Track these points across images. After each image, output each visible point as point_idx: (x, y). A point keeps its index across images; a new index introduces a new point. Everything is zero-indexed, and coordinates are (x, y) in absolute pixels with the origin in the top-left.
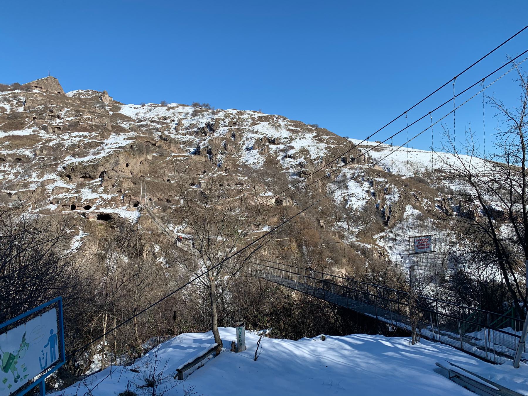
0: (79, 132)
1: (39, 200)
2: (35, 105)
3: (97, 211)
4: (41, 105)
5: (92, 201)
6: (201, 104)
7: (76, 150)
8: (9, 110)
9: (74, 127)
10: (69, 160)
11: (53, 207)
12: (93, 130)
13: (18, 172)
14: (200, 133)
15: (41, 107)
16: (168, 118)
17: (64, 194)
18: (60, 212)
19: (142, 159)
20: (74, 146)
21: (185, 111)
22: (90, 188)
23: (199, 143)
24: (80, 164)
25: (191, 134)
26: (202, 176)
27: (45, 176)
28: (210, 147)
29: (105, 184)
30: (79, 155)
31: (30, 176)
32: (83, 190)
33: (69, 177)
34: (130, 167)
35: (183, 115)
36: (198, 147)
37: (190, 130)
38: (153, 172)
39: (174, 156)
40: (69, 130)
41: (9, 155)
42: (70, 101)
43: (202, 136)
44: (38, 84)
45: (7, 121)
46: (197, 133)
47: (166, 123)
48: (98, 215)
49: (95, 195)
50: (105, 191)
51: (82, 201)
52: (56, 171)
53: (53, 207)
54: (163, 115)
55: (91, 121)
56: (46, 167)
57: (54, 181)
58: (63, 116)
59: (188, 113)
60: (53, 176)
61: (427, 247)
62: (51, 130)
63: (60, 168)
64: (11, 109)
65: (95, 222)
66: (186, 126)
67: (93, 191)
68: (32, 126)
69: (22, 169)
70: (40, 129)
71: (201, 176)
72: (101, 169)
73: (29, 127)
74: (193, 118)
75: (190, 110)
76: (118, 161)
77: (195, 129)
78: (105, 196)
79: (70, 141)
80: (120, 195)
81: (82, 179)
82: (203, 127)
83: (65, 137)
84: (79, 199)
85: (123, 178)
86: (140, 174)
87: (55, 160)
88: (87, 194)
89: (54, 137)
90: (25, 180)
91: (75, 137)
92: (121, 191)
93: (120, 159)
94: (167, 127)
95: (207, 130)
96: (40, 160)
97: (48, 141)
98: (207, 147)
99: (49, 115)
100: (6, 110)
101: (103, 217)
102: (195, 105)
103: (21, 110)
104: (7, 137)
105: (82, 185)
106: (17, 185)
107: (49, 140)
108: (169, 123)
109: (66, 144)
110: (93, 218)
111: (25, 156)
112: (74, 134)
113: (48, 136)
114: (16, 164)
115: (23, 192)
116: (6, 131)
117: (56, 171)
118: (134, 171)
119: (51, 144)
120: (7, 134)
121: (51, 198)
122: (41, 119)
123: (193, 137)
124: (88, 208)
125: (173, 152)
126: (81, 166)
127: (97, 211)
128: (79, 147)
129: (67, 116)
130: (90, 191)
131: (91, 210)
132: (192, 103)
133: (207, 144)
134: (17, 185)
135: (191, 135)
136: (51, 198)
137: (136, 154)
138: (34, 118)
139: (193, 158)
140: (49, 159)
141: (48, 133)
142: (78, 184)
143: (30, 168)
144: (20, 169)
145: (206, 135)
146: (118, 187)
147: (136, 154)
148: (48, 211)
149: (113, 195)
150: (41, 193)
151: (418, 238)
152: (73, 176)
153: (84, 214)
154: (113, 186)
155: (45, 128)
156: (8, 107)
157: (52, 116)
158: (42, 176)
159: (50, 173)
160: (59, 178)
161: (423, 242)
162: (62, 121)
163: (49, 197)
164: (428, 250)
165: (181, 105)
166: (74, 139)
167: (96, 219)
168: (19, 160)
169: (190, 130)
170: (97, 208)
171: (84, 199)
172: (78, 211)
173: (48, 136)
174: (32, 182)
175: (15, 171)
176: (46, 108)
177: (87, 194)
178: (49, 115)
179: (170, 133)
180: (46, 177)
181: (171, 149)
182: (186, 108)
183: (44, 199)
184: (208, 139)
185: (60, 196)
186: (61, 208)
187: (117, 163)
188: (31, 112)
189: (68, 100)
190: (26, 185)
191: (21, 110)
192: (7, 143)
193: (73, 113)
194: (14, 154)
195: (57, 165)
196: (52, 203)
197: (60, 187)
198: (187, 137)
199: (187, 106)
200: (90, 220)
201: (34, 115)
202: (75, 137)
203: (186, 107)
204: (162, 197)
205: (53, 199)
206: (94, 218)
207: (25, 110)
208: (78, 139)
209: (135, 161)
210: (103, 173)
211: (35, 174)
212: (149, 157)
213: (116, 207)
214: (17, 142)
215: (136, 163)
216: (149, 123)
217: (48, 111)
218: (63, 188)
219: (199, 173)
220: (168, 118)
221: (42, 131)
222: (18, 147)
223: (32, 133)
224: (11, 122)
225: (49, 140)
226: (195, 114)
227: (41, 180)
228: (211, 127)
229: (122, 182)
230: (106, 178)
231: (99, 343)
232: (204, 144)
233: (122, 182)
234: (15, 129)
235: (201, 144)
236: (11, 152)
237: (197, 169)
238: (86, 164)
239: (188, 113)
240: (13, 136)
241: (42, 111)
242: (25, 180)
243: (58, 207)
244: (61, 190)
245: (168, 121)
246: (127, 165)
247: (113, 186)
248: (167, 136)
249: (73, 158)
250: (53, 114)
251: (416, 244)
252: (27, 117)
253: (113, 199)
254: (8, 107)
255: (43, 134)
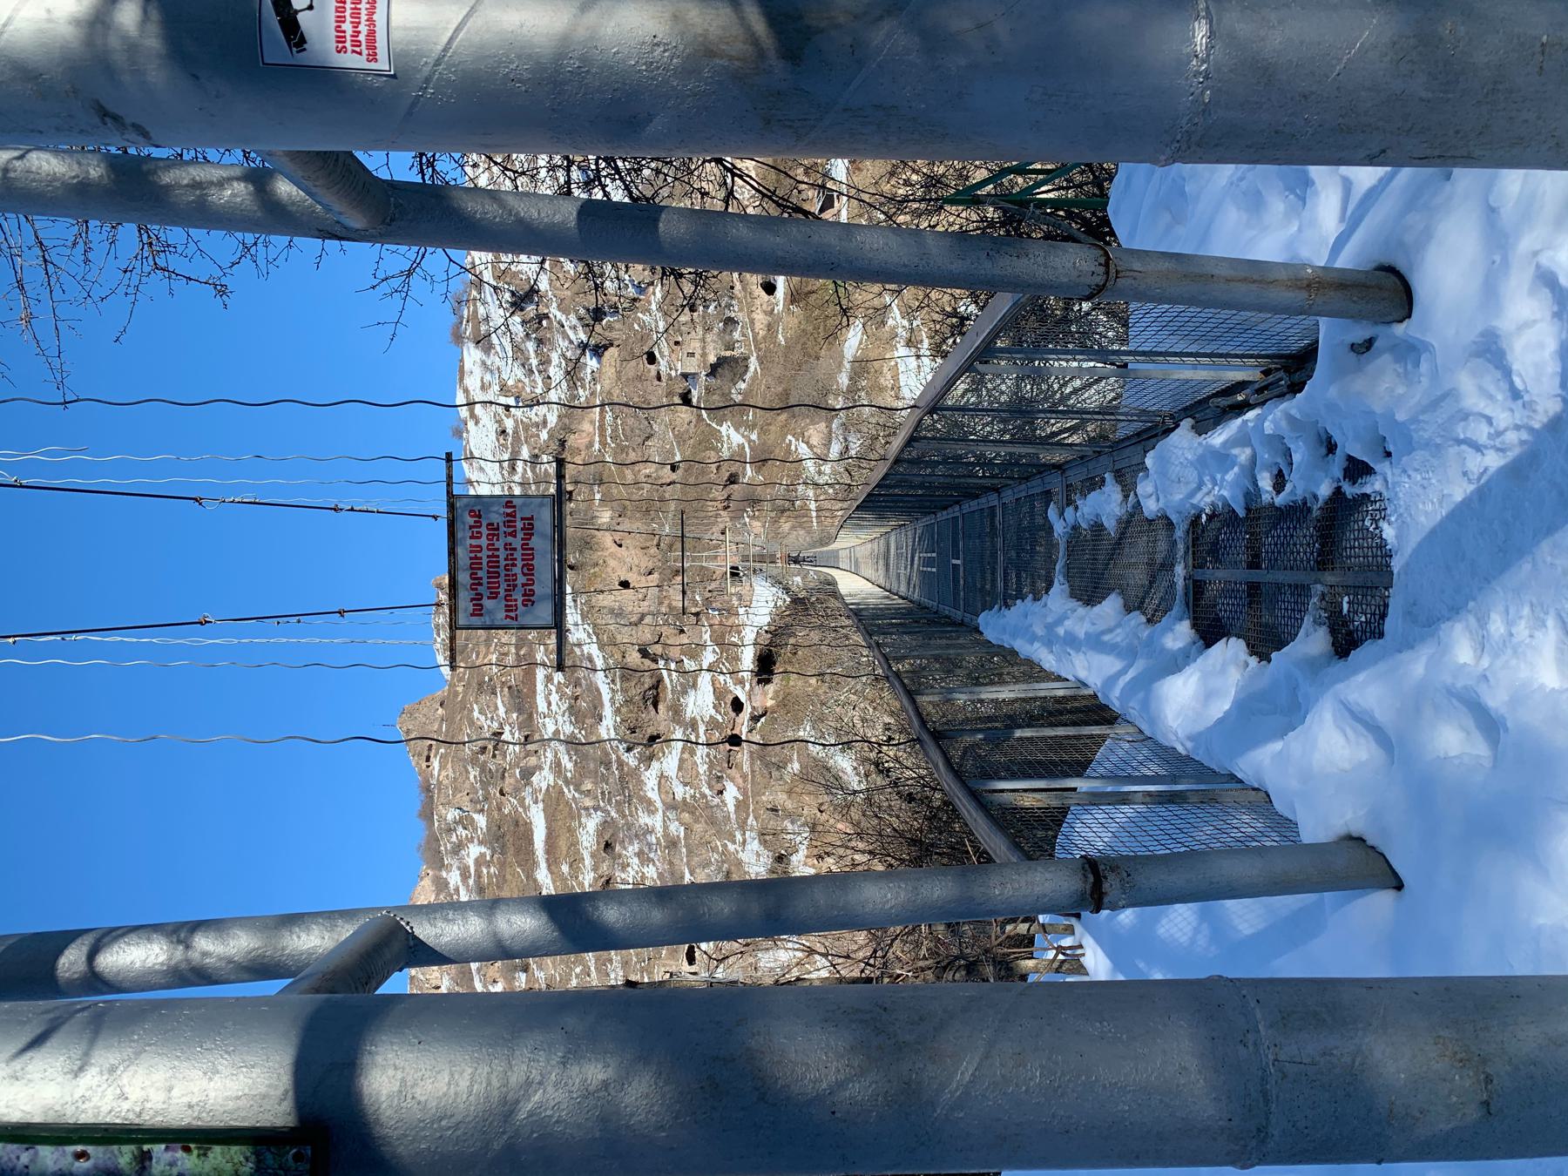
0: (535, 692)
1: (712, 821)
2: (467, 785)
3: (747, 687)
4: (467, 772)
5: (719, 693)
6: (454, 319)
7: (584, 710)
8: (483, 849)
9: (522, 700)
10: (607, 728)
11: (731, 793)
12: (531, 653)
13: (640, 854)
14: (541, 334)
15: (473, 773)
16: (500, 422)
17: (699, 761)
18: (744, 777)
19: (607, 539)
20: (572, 710)
21: (478, 371)
22: (684, 692)
23: (571, 342)
24: (617, 711)
25: (545, 362)
26: (663, 364)
27: (649, 794)
28: (582, 311)
29: (675, 653)
30: (597, 704)
31: (651, 831)
32: (689, 711)
33: (653, 739)
34: (632, 578)
35: (488, 377)
36: (584, 347)
37: (534, 362)
38: (648, 508)
39: (603, 443)
40: (531, 716)
41: (595, 869)
42: (460, 689)
43: (549, 328)
44: (420, 755)
45: (511, 858)
46: (540, 342)
47: (516, 432)
48: (759, 682)
49: (705, 680)
50: (695, 651)
51: (719, 718)
52: (638, 768)
53: (731, 793)
54: (493, 436)
55: (506, 654)
56: (627, 789)
57: (662, 777)
58: (495, 725)
59: (484, 363)
60: (650, 778)
61: (529, 530)
62: (533, 761)
63: (631, 760)
64: (481, 843)
65: (776, 692)
66: (519, 373)
67: (694, 686)
68: (522, 801)
69: (631, 843)
70: (529, 783)
71: (663, 368)
72: (634, 658)
73: (526, 809)
74: (498, 348)
75: (472, 356)
76: (612, 611)
77: (531, 346)
78: (709, 657)
79: (560, 719)
80: (708, 619)
81: (661, 707)
82: (524, 323)
83: (551, 728)
84: (713, 725)
85: (661, 603)
86: (653, 550)
87: (608, 765)
88: (701, 703)
89: (549, 755)
90: (658, 843)
91: (549, 704)
92: (697, 614)
93: (605, 603)
94: (526, 429)
95: (531, 310)
96: (610, 800)
97: (560, 772)
98: (580, 319)
99: (494, 756)
100: (483, 855)
101: (765, 666)
102: (458, 338)
103: (481, 821)
104: (549, 867)
105: (677, 711)
106: (671, 863)
107: (557, 767)
108: (516, 421)
109: (568, 729)
110: (767, 697)
111: (597, 831)
112: (542, 706)
113: (547, 768)
114: (620, 856)
115: (690, 852)
116: (535, 864)
117: (638, 768)
118: (643, 565)
119: (570, 766)
120: (543, 865)
121: (707, 792)
122: (503, 777)
123: (555, 357)
124: (737, 706)
125: (591, 444)
126: (624, 710)
127: (747, 687)
128: (576, 698)
129: (493, 714)
130: (692, 693)
131: (743, 699)
132: (453, 347)
133: (573, 320)
134: (671, 863)
135: (549, 362)
136: (707, 792)
137: (595, 557)
138: (502, 794)
139: (607, 387)
140: (605, 779)
141: (541, 768)
142: (673, 721)
143: (629, 826)
144: (634, 847)
145: (546, 316)
146: (685, 617)
147: (595, 557)
148: (741, 806)
149: (707, 637)
150: (693, 813)
151: (464, 597)
152: (651, 731)
153: (755, 719)
154: (682, 631)
155: (527, 774)
156: (474, 851)
157: (495, 748)
158: (650, 802)
159: (640, 783)
160: (655, 764)
161: (493, 561)
162: (507, 728)
163: (704, 796)
164: (545, 518)
165: (461, 380)
166: (554, 707)
167: (771, 688)
168: (608, 846)
169: (534, 362)
170: (741, 682)
171: (713, 712)
172: (745, 730)
173: (547, 768)
174: (666, 828)
175: (636, 860)
176: (474, 761)
177: (701, 703)
178: (494, 756)
179: (545, 422)
180: (653, 795)
181: (582, 447)
182: (468, 366)
183: (708, 806)
184: (559, 314)
185: (703, 769)
186: (733, 772)
187: (618, 613)
188: (486, 799)
189: (456, 694)
190: (672, 844)
191: (481, 821)
192: (565, 868)
193: (484, 698)
194: (593, 856)
195: (621, 764)
196: (721, 792)
197: (680, 768)
198: (556, 373)
199: (462, 360)
200: (770, 703)
201: (494, 791)
202: (549, 704)
203: (466, 368)
204: (718, 493)
205: (710, 787)
206: (765, 694)
207: (482, 811)
208: (554, 698)
209: (612, 563)
210: (644, 653)
211: (644, 819)
212: (605, 517)
213: (739, 632)
214: (563, 844)
215: (621, 560)
216: (517, 478)
217: (482, 758)
218: (682, 761)
219: (654, 373)
220: (500, 422)
221: (534, 779)
222: (574, 844)
223: (541, 805)
224: (511, 851)
225: (557, 767)
226: (483, 341)
227: (659, 804)
228: (524, 298)
229: (670, 606)
230: (658, 649)
231: (1133, 519)
232: (574, 328)
233: (670, 606)
234: (531, 842)
235: (573, 337)
236: (588, 861)
237: (639, 378)
238: (619, 697)
239: (484, 363)
240: (548, 852)
241: (483, 771)
242: (658, 843)
243: (732, 780)
244: (688, 765)
245: (509, 424)
246: (625, 585)
247: (682, 631)
248: (551, 436)
249: (604, 722)
250: (490, 747)
251: (500, 616)
252: (500, 809)
253: (720, 642)
254: (474, 851)
255: (544, 779)
